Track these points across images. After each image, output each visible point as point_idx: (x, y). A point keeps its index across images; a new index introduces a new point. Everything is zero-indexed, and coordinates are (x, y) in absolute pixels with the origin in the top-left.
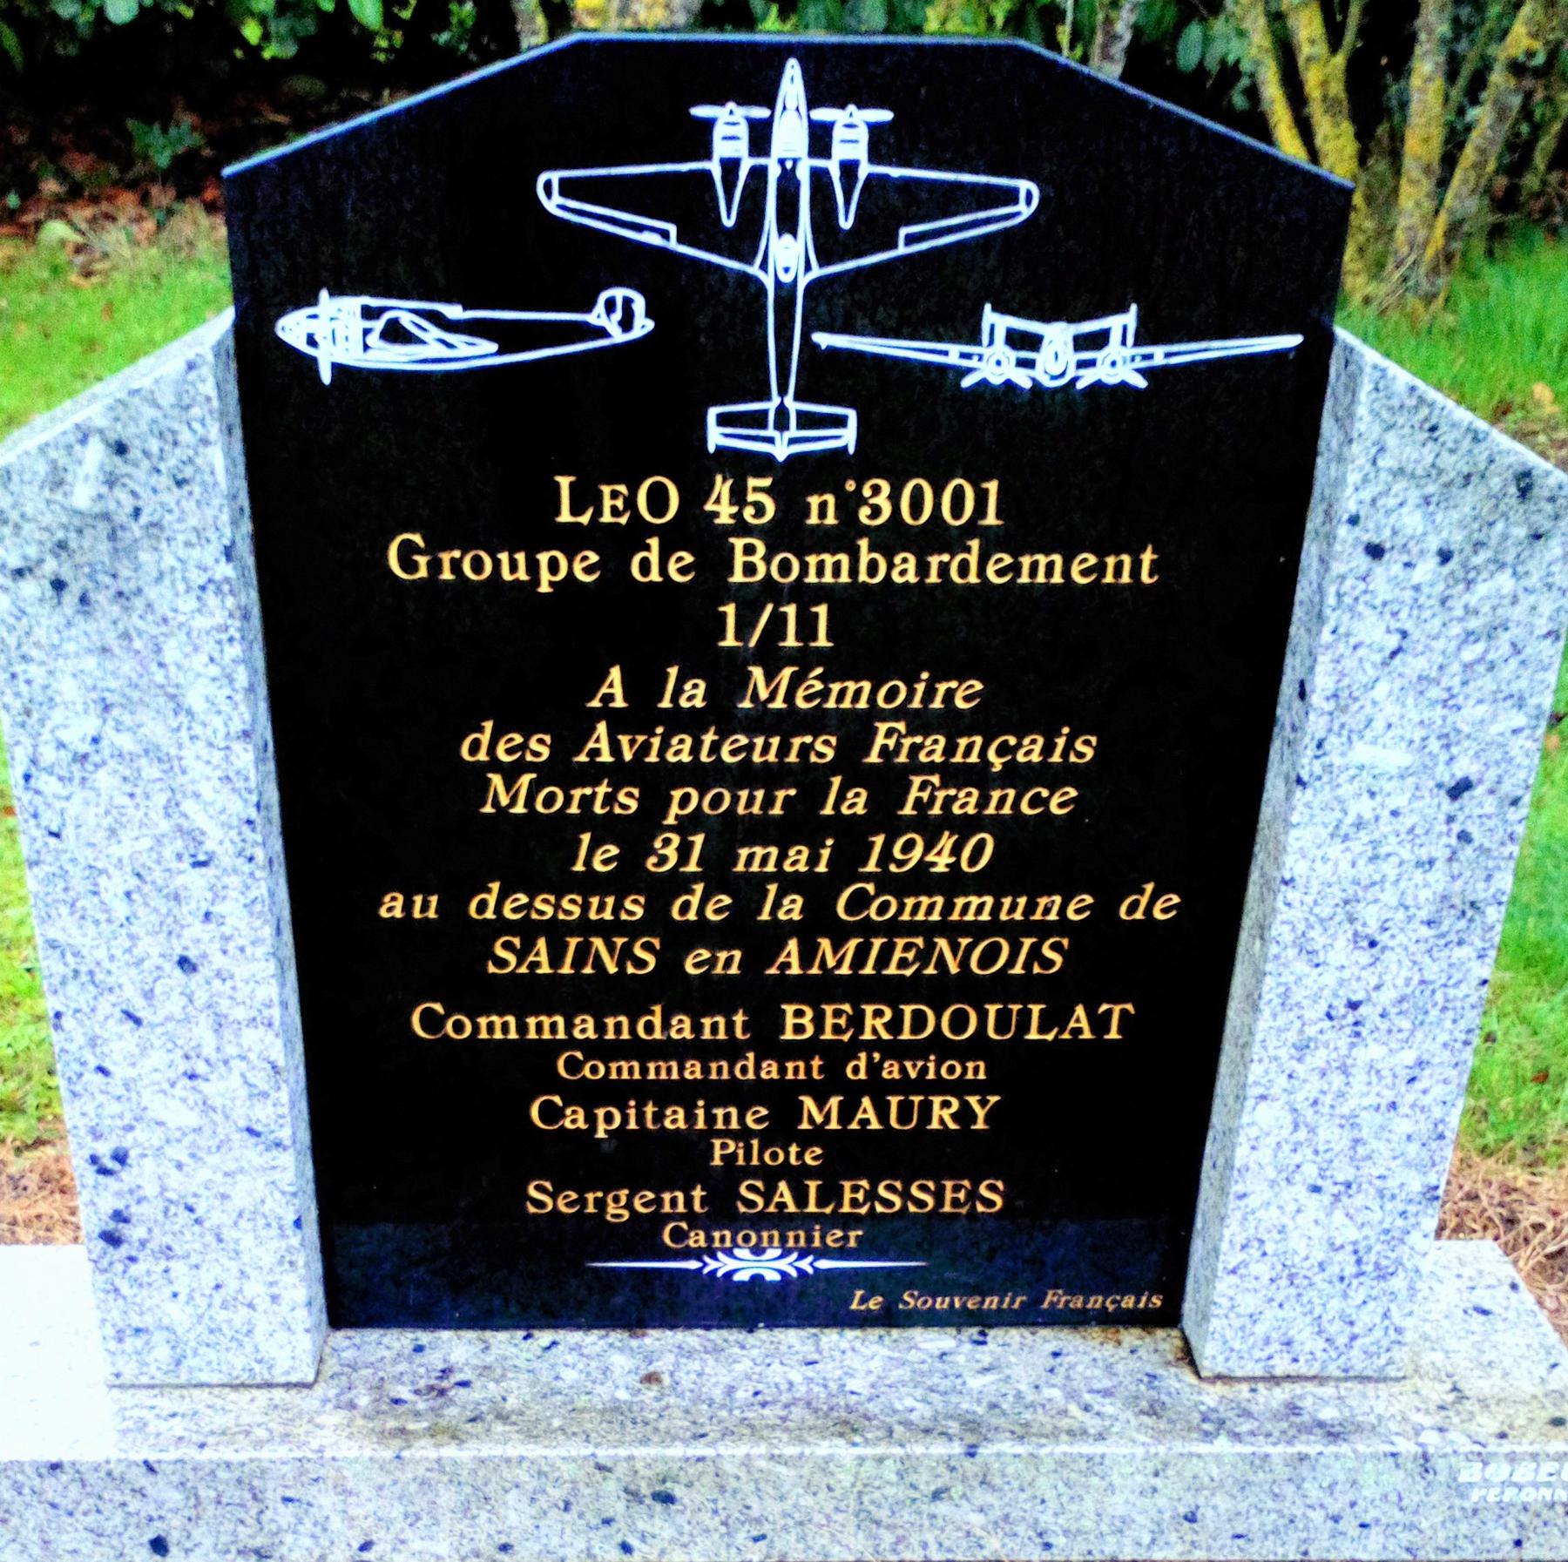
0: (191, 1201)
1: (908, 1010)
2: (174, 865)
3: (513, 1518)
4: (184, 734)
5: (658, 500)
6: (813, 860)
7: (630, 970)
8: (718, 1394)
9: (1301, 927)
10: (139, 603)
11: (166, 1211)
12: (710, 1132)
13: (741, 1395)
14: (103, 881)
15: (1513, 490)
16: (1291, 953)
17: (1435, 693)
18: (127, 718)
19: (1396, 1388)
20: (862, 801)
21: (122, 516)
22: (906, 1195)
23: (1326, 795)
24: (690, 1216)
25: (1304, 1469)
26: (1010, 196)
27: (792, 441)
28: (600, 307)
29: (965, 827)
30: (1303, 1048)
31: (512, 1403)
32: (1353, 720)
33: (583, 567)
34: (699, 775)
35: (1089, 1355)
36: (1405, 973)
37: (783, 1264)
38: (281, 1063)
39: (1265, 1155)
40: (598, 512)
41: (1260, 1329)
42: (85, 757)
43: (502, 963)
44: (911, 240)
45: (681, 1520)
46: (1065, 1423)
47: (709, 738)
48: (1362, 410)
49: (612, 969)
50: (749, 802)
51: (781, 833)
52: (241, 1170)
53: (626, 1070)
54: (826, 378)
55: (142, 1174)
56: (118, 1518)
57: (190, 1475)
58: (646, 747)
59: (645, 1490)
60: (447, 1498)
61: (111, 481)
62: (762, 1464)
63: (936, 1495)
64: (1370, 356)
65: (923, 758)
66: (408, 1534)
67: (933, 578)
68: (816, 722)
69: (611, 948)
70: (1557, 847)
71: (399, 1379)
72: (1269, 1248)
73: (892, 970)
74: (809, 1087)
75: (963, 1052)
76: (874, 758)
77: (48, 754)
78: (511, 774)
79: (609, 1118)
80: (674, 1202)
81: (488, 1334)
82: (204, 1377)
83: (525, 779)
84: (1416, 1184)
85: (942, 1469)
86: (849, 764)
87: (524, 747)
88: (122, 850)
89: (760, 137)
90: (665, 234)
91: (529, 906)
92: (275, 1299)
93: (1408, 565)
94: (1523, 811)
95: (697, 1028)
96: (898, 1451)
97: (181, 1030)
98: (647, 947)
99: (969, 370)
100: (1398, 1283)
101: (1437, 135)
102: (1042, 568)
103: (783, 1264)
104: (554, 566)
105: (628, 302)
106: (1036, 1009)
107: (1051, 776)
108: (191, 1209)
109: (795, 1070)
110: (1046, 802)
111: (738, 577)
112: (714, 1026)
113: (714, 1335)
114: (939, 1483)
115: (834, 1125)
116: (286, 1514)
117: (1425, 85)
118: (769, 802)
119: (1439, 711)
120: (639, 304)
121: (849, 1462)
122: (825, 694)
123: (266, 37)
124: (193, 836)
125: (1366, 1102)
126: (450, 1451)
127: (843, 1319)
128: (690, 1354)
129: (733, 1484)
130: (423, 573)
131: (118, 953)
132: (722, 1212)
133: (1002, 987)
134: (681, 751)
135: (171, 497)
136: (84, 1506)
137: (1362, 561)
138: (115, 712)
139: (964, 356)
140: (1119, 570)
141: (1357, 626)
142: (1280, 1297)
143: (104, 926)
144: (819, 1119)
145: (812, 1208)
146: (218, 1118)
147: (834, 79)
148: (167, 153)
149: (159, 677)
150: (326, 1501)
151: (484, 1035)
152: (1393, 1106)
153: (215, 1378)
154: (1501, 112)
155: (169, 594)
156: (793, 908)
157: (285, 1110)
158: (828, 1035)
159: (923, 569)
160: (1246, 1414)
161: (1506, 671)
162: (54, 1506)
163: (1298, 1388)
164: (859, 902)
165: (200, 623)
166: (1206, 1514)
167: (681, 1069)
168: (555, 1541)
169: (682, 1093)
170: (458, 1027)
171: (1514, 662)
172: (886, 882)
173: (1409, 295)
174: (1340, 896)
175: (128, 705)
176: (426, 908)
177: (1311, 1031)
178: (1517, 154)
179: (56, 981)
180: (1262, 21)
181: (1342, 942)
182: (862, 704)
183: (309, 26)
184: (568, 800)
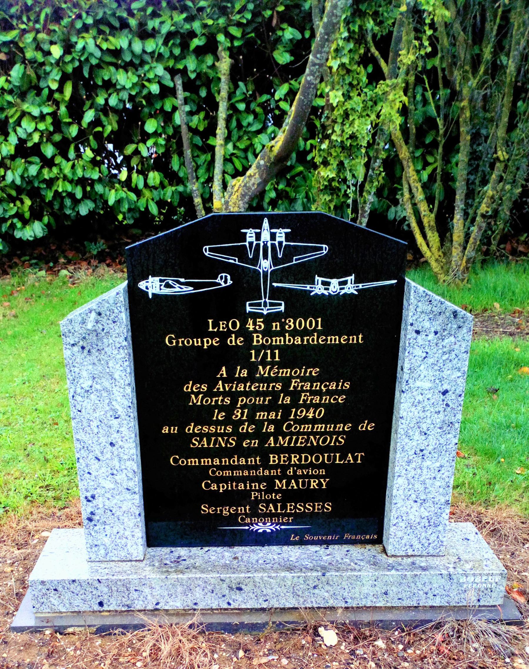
0: (111, 509)
1: (303, 455)
2: (110, 418)
3: (198, 595)
4: (113, 385)
5: (234, 325)
6: (277, 416)
7: (229, 446)
8: (254, 562)
9: (406, 430)
10: (103, 352)
11: (105, 512)
12: (251, 490)
13: (260, 562)
14: (91, 423)
15: (452, 316)
16: (404, 437)
17: (436, 368)
18: (99, 381)
19: (442, 558)
20: (289, 400)
21: (99, 331)
22: (305, 507)
23: (410, 395)
24: (246, 514)
25: (417, 579)
26: (321, 249)
27: (268, 310)
28: (219, 278)
29: (316, 406)
30: (409, 462)
31: (197, 564)
32: (416, 375)
33: (215, 342)
34: (246, 394)
35: (356, 551)
36: (435, 442)
37: (271, 527)
38: (136, 470)
39: (401, 492)
40: (219, 328)
41: (403, 542)
42: (88, 391)
43: (194, 444)
44: (296, 260)
45: (244, 595)
46: (350, 567)
47: (248, 384)
48: (412, 297)
49: (224, 445)
50: (259, 401)
51: (268, 409)
52: (125, 500)
53: (227, 473)
54: (276, 294)
55: (99, 501)
56: (90, 596)
57: (110, 583)
58: (232, 387)
59: (234, 587)
60: (180, 589)
61: (97, 322)
62: (266, 578)
63: (315, 587)
64: (413, 284)
65: (304, 388)
66: (169, 600)
67: (305, 343)
68: (276, 380)
69: (223, 440)
70: (495, 424)
71: (166, 559)
72: (404, 518)
73: (299, 445)
74: (277, 477)
75: (319, 467)
76: (292, 389)
77: (79, 390)
78: (197, 395)
79: (223, 487)
80: (241, 510)
81: (191, 548)
82: (113, 559)
83: (201, 396)
84: (443, 500)
85: (316, 580)
86: (285, 390)
87: (200, 387)
88: (97, 415)
89: (258, 236)
90: (235, 260)
91: (201, 429)
92: (133, 536)
93: (426, 335)
94: (463, 398)
95: (247, 461)
96: (304, 574)
97: (110, 462)
98: (233, 440)
99: (313, 291)
100: (440, 528)
101: (462, 235)
102: (333, 340)
103: (271, 527)
104: (208, 342)
105: (226, 277)
106: (338, 455)
107: (338, 393)
108: (111, 511)
109: (273, 472)
110: (337, 399)
111: (255, 343)
112: (251, 461)
113: (253, 547)
114: (315, 584)
115: (284, 488)
116: (135, 595)
117: (458, 221)
118: (264, 400)
119: (438, 372)
120: (229, 277)
121: (290, 578)
122: (278, 372)
123: (124, 218)
124: (115, 411)
125: (427, 477)
126: (180, 576)
127: (287, 542)
128: (246, 552)
129: (258, 584)
130: (174, 344)
131: (94, 442)
132: (254, 513)
133: (328, 449)
134: (241, 388)
135: (111, 326)
136: (81, 593)
137: (415, 335)
138: (96, 379)
139: (310, 287)
140: (353, 340)
141: (414, 351)
142: (408, 533)
143: (91, 435)
144: (280, 486)
145: (279, 511)
146: (119, 486)
147: (276, 222)
148: (96, 250)
149: (108, 370)
150: (147, 590)
151: (189, 464)
152: (435, 478)
153: (116, 559)
154: (480, 228)
155: (111, 350)
156: (272, 429)
157: (137, 483)
158: (282, 463)
159: (302, 341)
160: (400, 565)
161: (455, 362)
162: (73, 592)
163: (415, 558)
164: (289, 426)
165: (119, 356)
166: (390, 592)
167: (243, 473)
168: (209, 602)
169: (243, 480)
170: (183, 462)
171: (456, 360)
172: (296, 421)
173: (457, 279)
174: (415, 421)
175: (100, 378)
176: (175, 430)
177: (411, 458)
178: (486, 240)
179: (78, 449)
180: (410, 206)
181: (417, 434)
182: (288, 375)
183: (137, 215)
184: (212, 401)
